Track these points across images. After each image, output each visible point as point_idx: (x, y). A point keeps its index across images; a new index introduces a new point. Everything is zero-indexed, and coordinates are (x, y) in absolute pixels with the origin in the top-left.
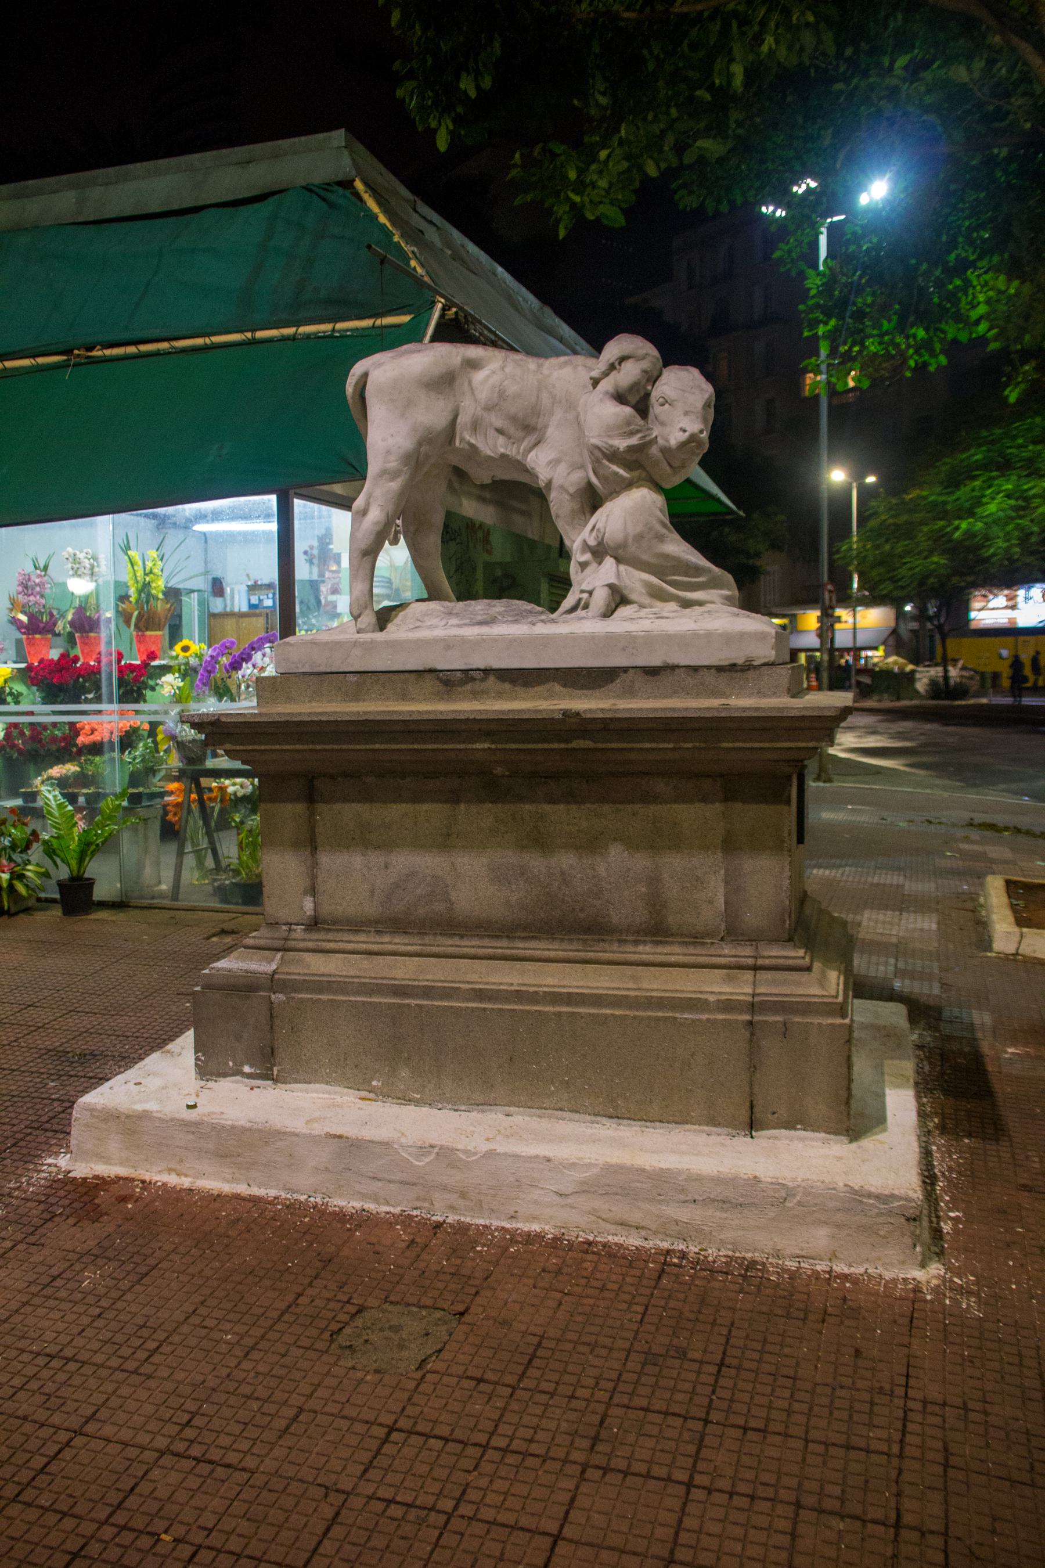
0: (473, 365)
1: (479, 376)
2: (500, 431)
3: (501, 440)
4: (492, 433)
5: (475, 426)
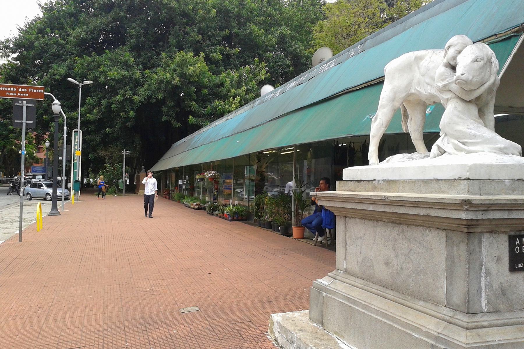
0: (418, 59)
1: (423, 64)
2: (428, 84)
3: (429, 87)
4: (425, 85)
5: (419, 84)
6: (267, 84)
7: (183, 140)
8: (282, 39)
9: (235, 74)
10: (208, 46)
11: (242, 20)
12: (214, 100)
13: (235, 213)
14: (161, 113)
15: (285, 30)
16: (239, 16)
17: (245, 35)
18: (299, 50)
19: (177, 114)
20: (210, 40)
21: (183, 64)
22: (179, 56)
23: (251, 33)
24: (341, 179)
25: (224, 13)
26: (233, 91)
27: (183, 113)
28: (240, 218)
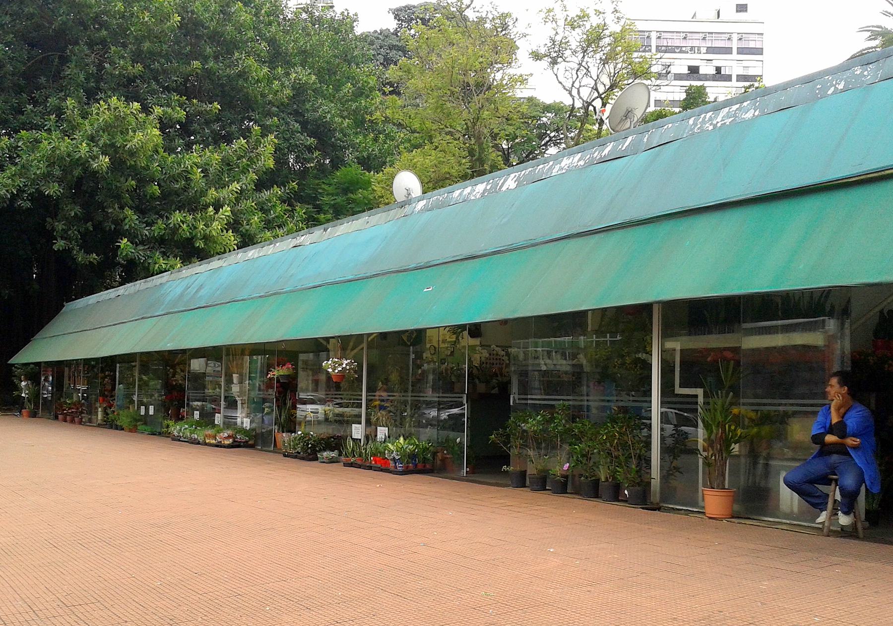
6: (416, 174)
7: (92, 299)
8: (299, 90)
9: (214, 157)
10: (153, 92)
11: (227, 47)
12: (170, 211)
13: (412, 456)
14: (50, 237)
15: (302, 74)
16: (215, 37)
17: (229, 76)
18: (329, 116)
19: (84, 235)
20: (157, 81)
21: (118, 126)
22: (111, 107)
23: (243, 75)
24: (208, 360)
25: (191, 27)
26: (212, 193)
27: (103, 239)
28: (420, 466)
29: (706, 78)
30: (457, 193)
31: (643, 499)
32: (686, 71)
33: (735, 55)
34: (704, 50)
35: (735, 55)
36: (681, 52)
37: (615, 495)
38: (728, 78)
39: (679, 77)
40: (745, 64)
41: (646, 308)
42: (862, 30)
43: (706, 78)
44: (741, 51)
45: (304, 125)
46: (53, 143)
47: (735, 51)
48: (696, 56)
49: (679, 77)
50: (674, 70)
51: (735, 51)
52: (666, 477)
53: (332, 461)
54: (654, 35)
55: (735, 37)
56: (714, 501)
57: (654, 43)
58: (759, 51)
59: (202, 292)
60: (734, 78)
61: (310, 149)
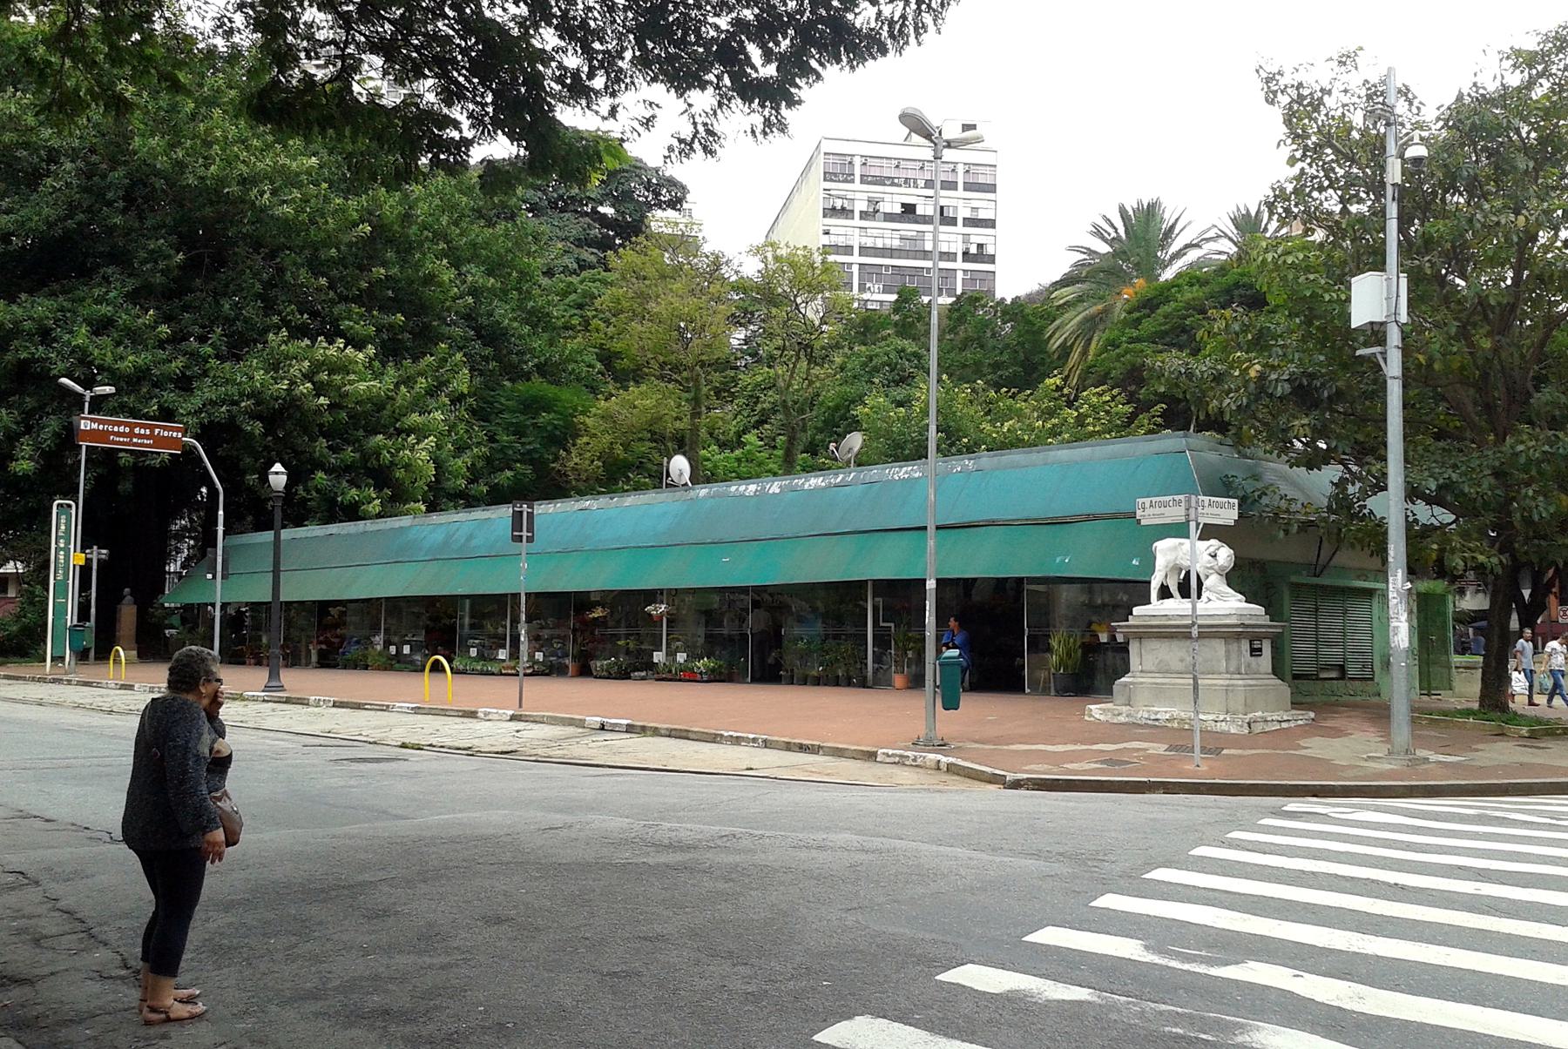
13: (713, 670)
29: (926, 220)
30: (733, 489)
31: (863, 684)
32: (898, 209)
33: (960, 193)
34: (921, 183)
35: (960, 193)
36: (893, 184)
37: (849, 684)
38: (952, 222)
39: (890, 217)
40: (975, 204)
41: (862, 584)
42: (1072, 249)
43: (926, 220)
44: (969, 187)
45: (478, 330)
46: (254, 373)
47: (960, 186)
48: (912, 190)
49: (890, 217)
50: (885, 207)
51: (960, 186)
52: (875, 672)
53: (643, 679)
54: (857, 161)
55: (961, 169)
56: (898, 680)
57: (857, 172)
58: (991, 188)
59: (474, 542)
60: (960, 222)
61: (486, 359)
